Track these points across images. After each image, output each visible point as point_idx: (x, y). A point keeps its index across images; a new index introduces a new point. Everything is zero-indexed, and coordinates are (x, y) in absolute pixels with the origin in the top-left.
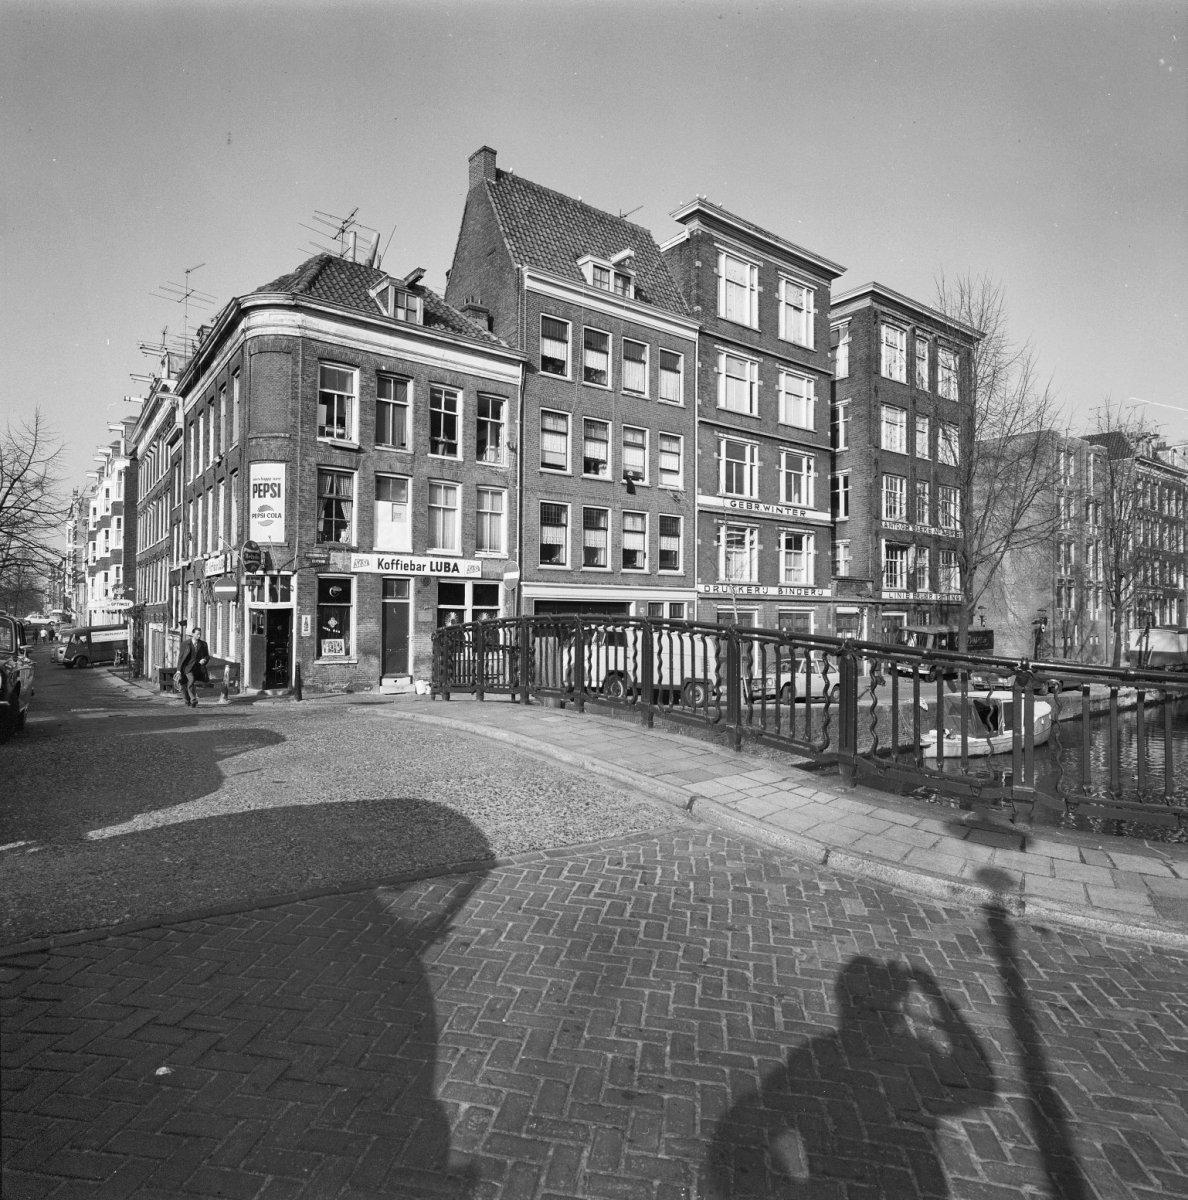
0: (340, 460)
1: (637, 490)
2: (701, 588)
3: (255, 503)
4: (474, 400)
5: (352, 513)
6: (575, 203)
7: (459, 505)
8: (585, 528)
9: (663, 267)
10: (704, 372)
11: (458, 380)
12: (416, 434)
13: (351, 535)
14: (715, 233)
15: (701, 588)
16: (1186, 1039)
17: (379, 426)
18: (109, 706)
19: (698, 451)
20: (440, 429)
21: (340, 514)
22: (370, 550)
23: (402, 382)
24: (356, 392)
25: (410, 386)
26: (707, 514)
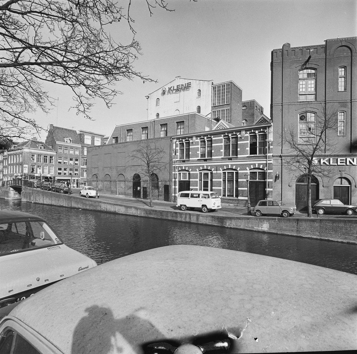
0: (34, 164)
1: (109, 3)
2: (81, 178)
3: (24, 169)
4: (50, 157)
5: (35, 170)
6: (64, 129)
7: (48, 168)
8: (64, 170)
9: (77, 136)
10: (82, 151)
11: (48, 154)
12: (42, 161)
13: (35, 172)
14: (84, 133)
15: (81, 178)
16: (356, 235)
17: (38, 160)
18: (27, 234)
19: (81, 161)
20: (45, 160)
21: (33, 170)
22: (37, 173)
23: (41, 155)
24: (36, 157)
25: (42, 156)
26: (82, 168)
